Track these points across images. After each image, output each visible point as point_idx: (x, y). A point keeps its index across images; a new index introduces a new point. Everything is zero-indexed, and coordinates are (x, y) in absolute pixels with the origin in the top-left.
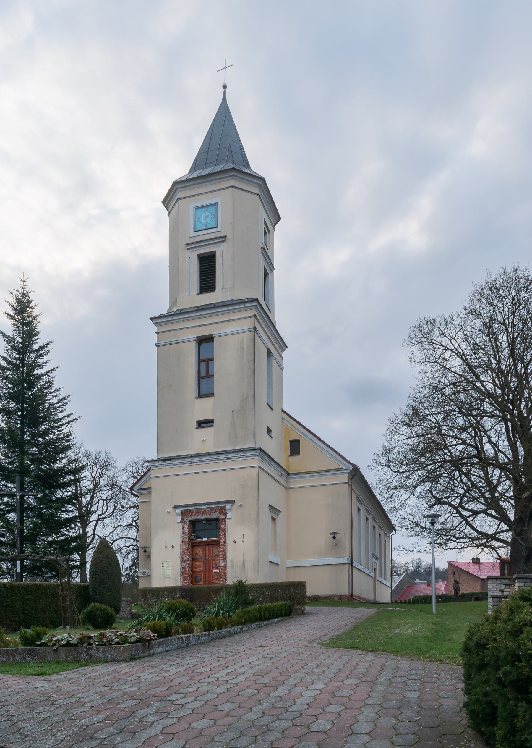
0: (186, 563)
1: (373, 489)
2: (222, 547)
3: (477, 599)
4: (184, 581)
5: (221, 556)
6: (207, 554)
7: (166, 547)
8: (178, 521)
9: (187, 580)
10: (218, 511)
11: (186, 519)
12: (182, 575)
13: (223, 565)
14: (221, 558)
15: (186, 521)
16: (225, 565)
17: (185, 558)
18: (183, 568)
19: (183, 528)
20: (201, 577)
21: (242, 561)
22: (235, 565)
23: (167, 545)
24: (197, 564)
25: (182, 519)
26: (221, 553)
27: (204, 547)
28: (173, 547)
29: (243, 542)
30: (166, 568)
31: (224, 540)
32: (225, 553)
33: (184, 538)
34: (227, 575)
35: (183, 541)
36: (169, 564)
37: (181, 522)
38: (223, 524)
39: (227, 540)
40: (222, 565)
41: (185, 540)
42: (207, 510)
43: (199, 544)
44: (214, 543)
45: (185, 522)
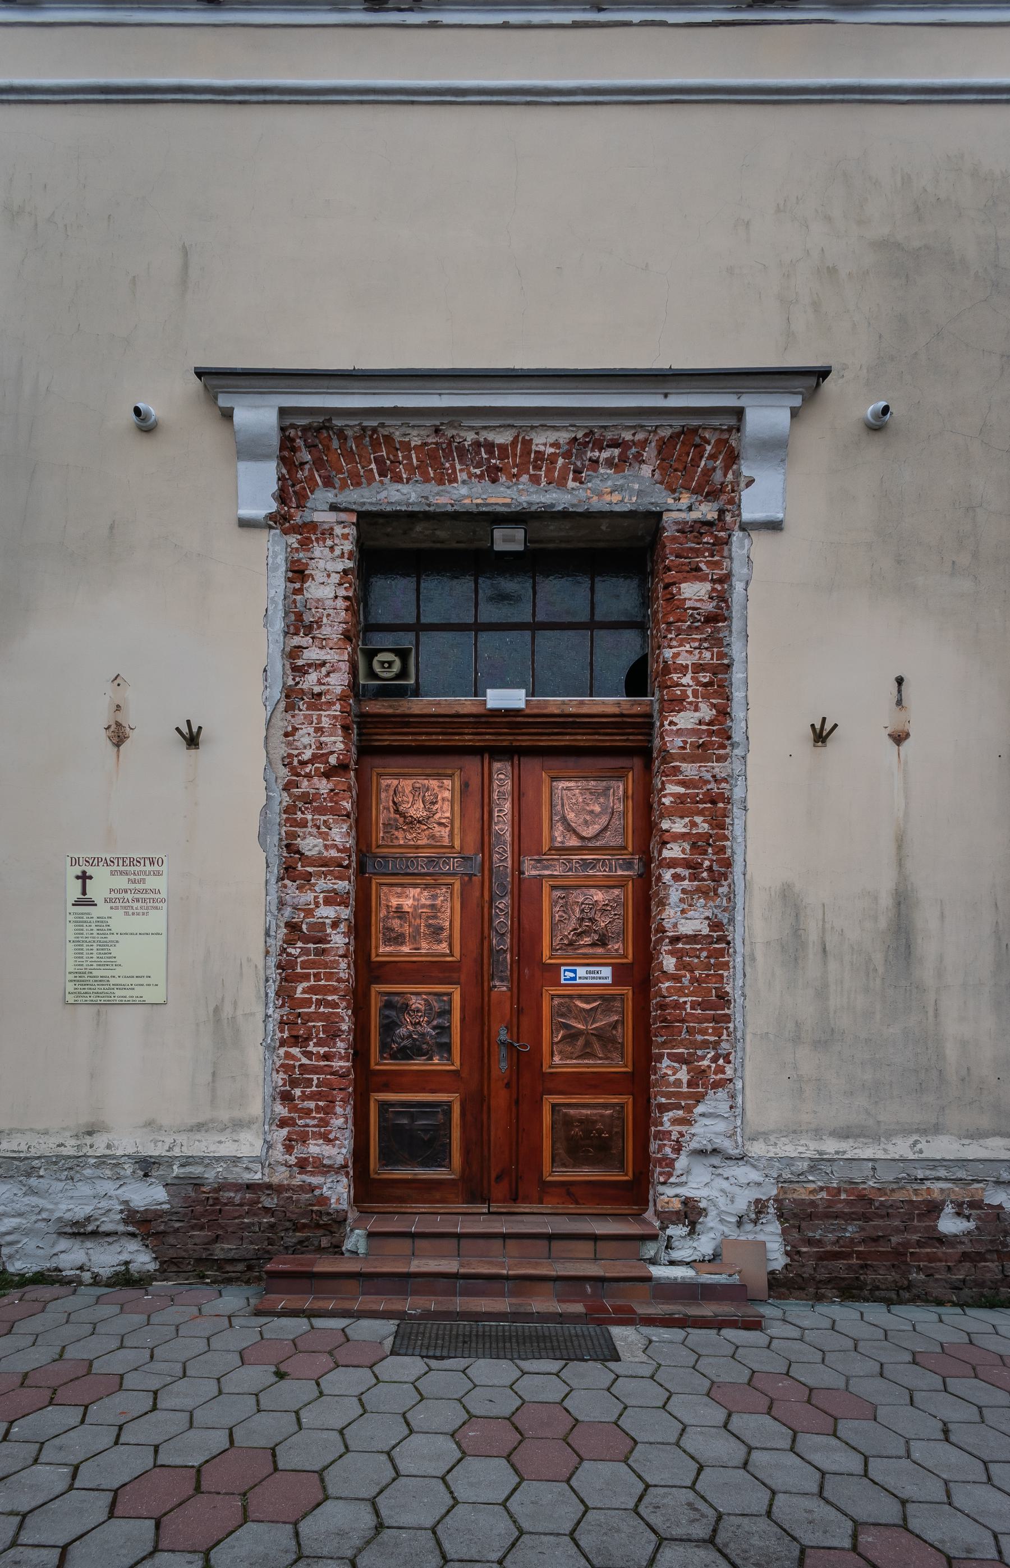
0: (322, 884)
1: (510, 620)
2: (690, 770)
3: (720, 1520)
4: (295, 1040)
5: (673, 851)
6: (503, 826)
7: (118, 736)
8: (246, 512)
9: (333, 1034)
10: (650, 453)
11: (322, 497)
12: (284, 994)
13: (693, 924)
14: (673, 863)
15: (324, 517)
16: (716, 925)
17: (310, 845)
18: (293, 927)
19: (298, 573)
20: (447, 1012)
21: (886, 901)
22: (813, 936)
23: (130, 718)
24: (408, 904)
25: (282, 497)
26: (678, 826)
27: (472, 765)
28: (192, 740)
29: (899, 738)
30: (119, 921)
31: (706, 712)
32: (719, 822)
33: (300, 671)
34: (735, 1011)
35: (292, 696)
36: (152, 882)
37: (279, 521)
38: (694, 573)
39: (737, 711)
40: (687, 928)
41: (310, 681)
42: (542, 441)
43: (440, 740)
44: (583, 740)
45: (312, 526)
